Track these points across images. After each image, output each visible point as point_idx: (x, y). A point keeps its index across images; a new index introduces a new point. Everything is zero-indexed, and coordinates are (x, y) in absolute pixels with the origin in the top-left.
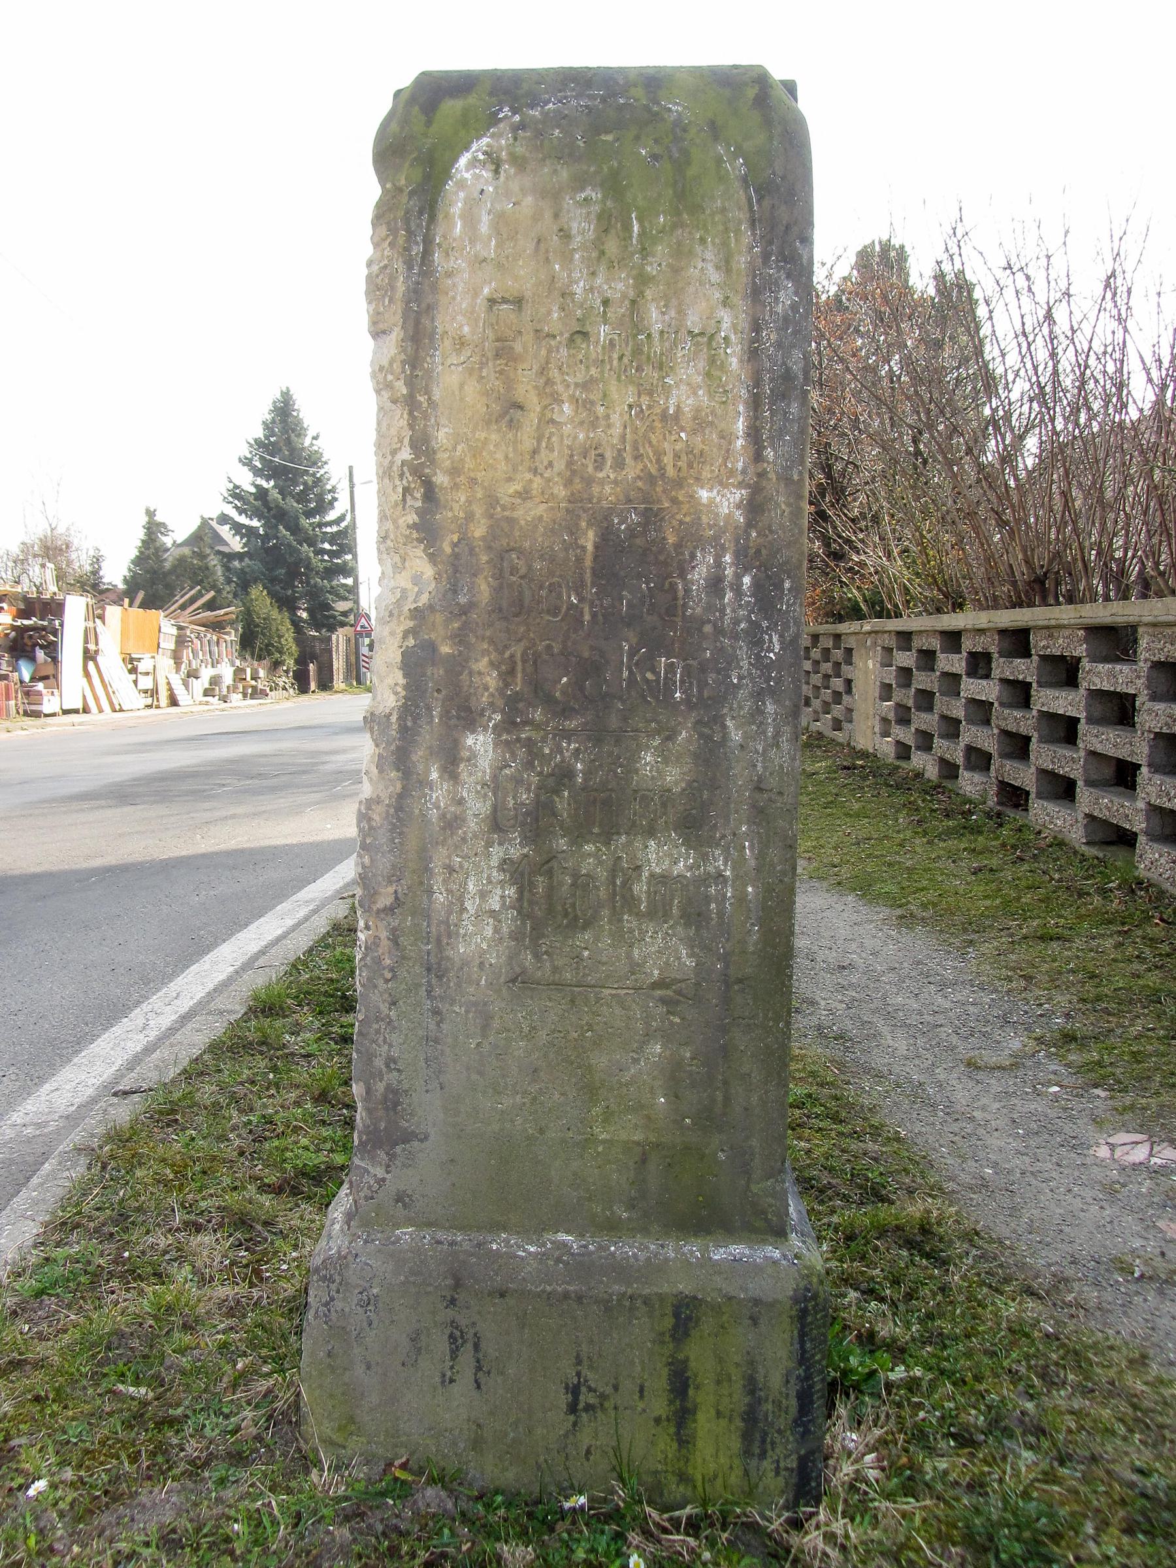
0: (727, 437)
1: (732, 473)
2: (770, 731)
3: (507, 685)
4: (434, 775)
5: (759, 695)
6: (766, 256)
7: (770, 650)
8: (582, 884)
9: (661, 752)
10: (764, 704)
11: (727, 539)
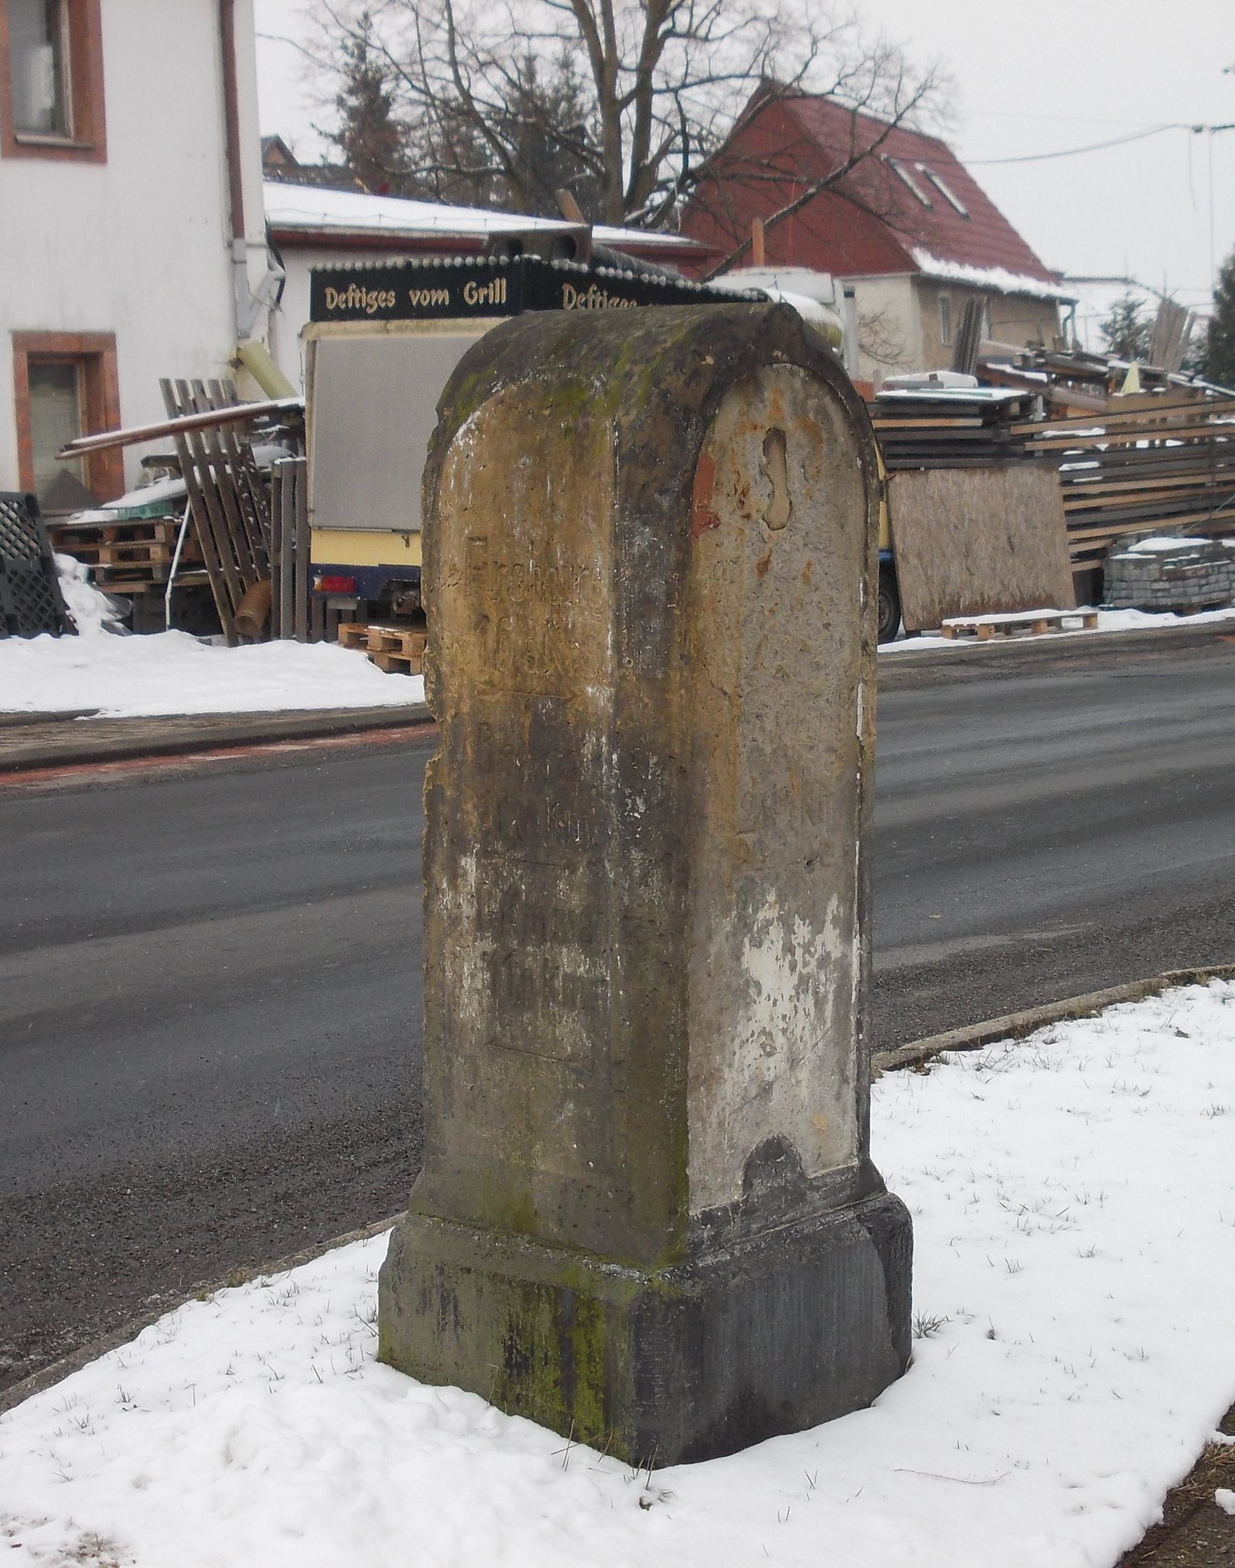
0: (601, 647)
1: (605, 674)
2: (637, 872)
3: (483, 823)
4: (445, 886)
5: (625, 846)
6: (622, 510)
7: (634, 810)
8: (526, 976)
9: (570, 883)
10: (629, 851)
11: (603, 725)
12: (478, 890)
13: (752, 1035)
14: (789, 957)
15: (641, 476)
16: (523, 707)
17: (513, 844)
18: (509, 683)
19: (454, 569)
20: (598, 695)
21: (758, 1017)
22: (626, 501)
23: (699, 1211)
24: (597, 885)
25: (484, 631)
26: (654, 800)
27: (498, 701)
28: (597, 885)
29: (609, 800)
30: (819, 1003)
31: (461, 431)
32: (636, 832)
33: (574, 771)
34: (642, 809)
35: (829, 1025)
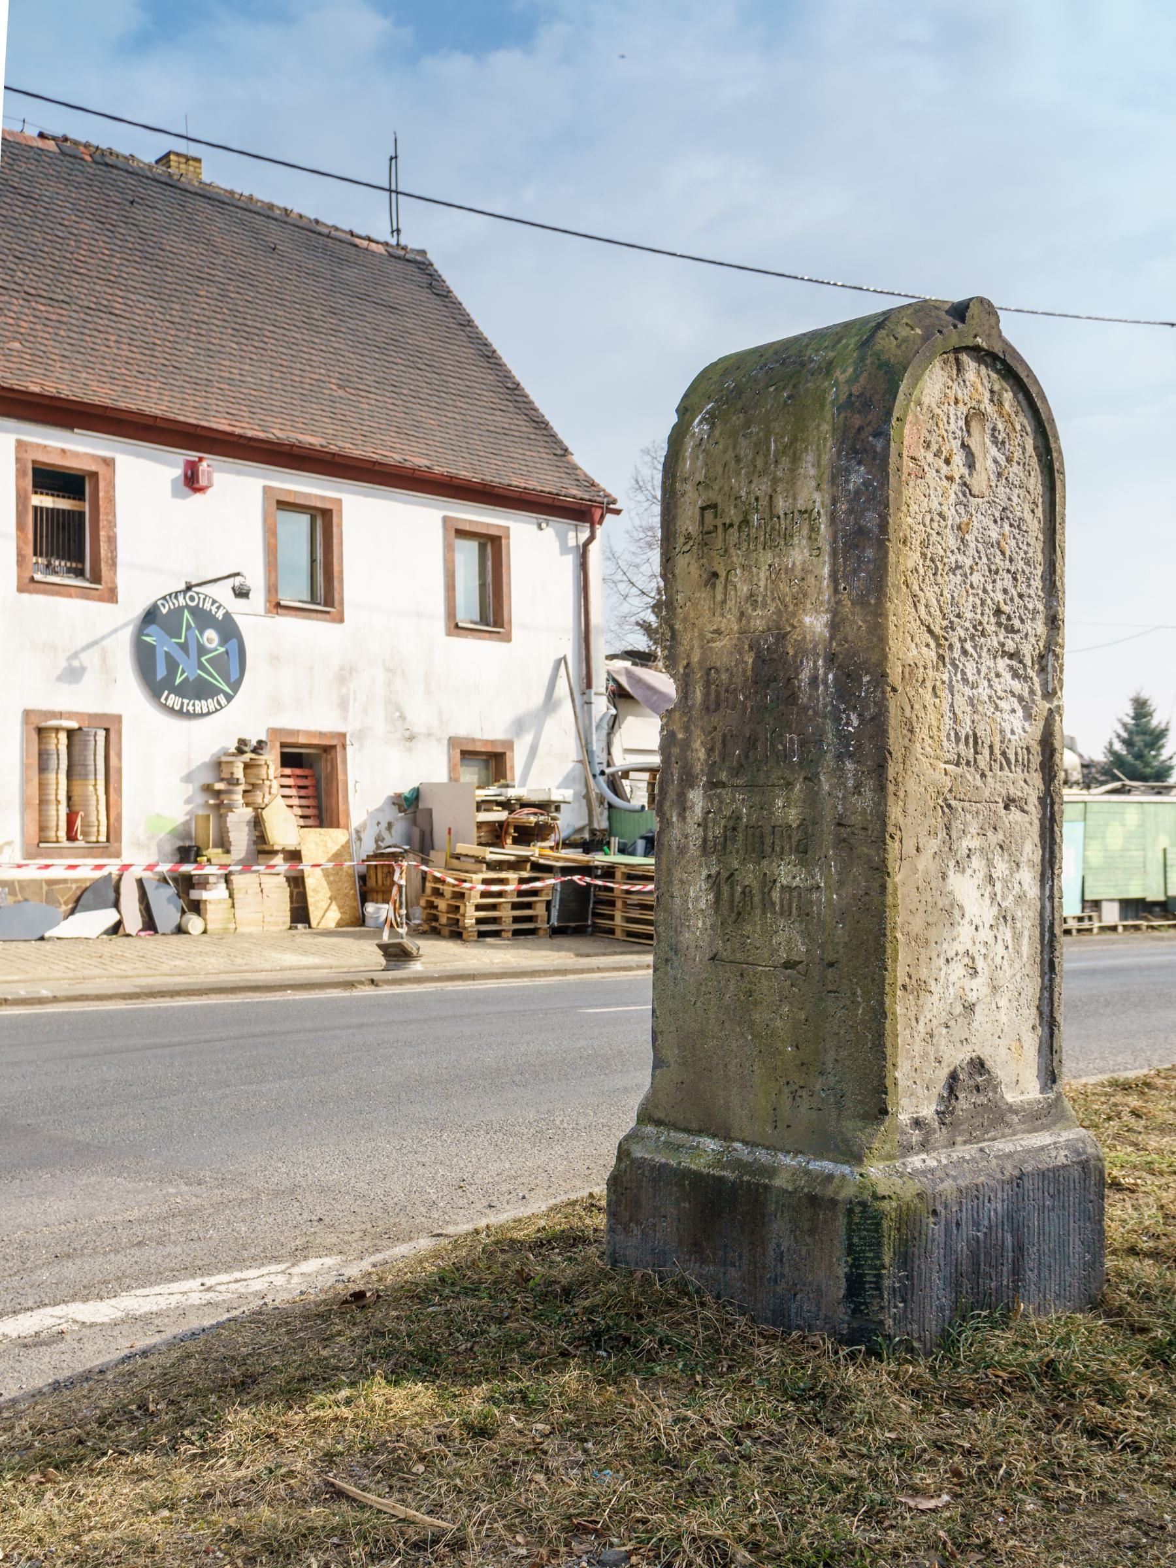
4: (674, 819)
5: (839, 757)
6: (839, 452)
8: (746, 892)
10: (843, 763)
12: (705, 819)
13: (957, 955)
14: (989, 888)
15: (857, 421)
16: (746, 647)
17: (736, 772)
18: (736, 627)
19: (689, 537)
20: (815, 623)
21: (962, 939)
22: (843, 443)
23: (907, 1116)
24: (812, 799)
25: (714, 586)
26: (867, 715)
27: (724, 646)
28: (812, 799)
29: (825, 717)
30: (1017, 937)
31: (697, 421)
32: (850, 745)
33: (792, 698)
34: (856, 723)
35: (1025, 959)
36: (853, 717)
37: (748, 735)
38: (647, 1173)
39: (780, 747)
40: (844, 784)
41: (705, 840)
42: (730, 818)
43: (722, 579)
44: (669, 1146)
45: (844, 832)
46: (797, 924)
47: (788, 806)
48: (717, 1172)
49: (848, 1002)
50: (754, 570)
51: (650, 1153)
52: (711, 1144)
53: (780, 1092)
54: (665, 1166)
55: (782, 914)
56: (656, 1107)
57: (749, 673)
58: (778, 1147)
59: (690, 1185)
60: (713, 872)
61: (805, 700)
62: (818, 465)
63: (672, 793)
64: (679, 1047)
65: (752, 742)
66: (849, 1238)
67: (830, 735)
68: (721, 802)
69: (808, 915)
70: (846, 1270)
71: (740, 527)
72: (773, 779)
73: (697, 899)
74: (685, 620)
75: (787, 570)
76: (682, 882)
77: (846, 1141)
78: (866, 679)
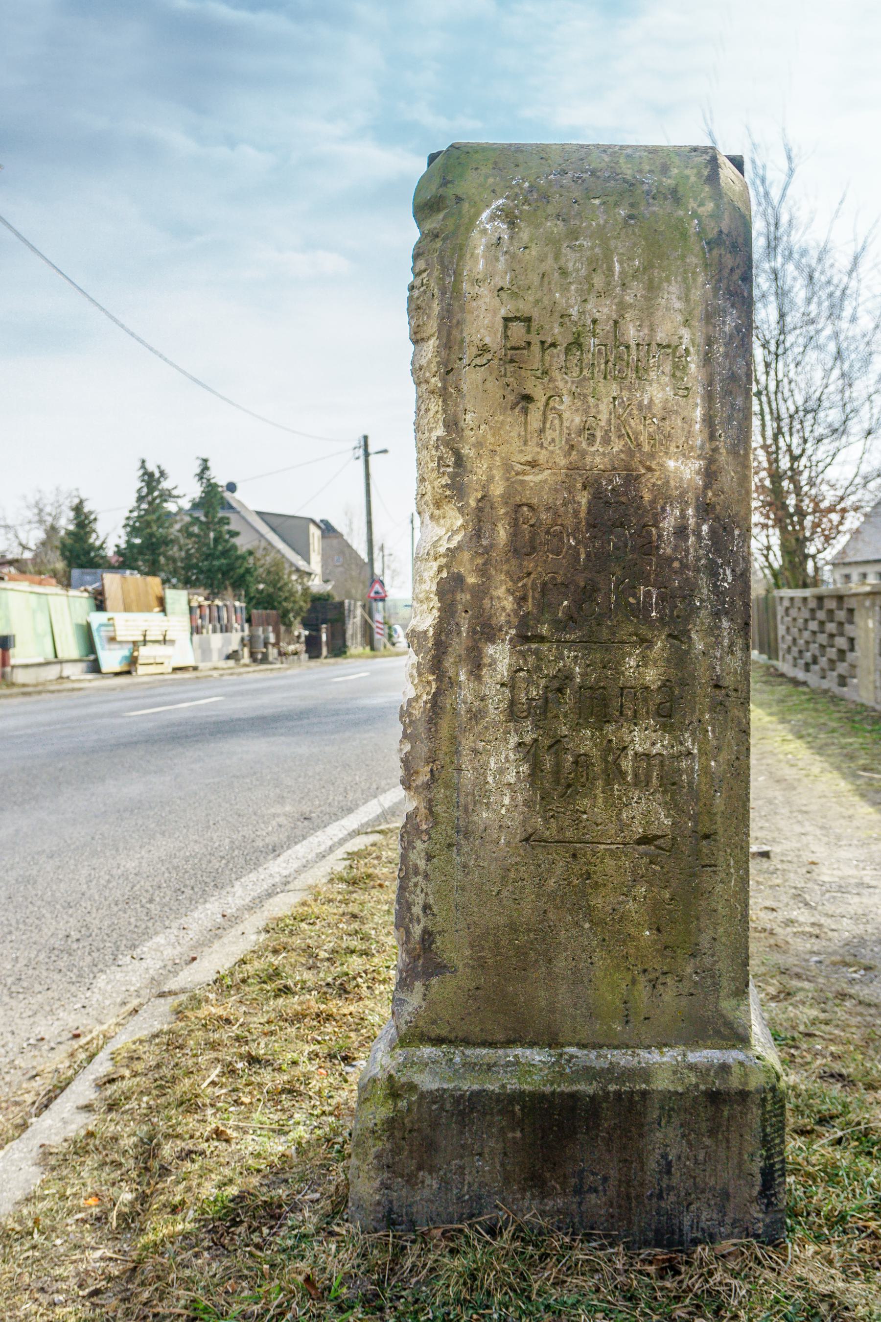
4: (462, 678)
5: (717, 615)
6: (716, 290)
10: (720, 621)
12: (513, 678)
16: (579, 486)
19: (484, 349)
22: (720, 280)
25: (525, 411)
27: (546, 481)
34: (730, 579)
36: (728, 572)
37: (582, 584)
38: (448, 1106)
39: (631, 600)
40: (721, 643)
41: (512, 703)
42: (555, 677)
43: (541, 404)
44: (470, 1066)
45: (720, 694)
46: (658, 795)
47: (645, 665)
48: (565, 1088)
49: (724, 875)
50: (591, 401)
51: (449, 1081)
52: (537, 1056)
53: (634, 982)
54: (477, 1095)
55: (635, 785)
56: (434, 1022)
57: (583, 515)
58: (631, 1044)
59: (522, 1110)
60: (528, 739)
61: (669, 551)
62: (686, 298)
63: (458, 645)
64: (472, 947)
65: (589, 593)
66: (764, 1130)
67: (705, 591)
68: (539, 659)
69: (674, 784)
70: (762, 1164)
71: (568, 350)
72: (622, 634)
73: (501, 771)
74: (479, 445)
75: (640, 407)
76: (475, 751)
77: (728, 1024)
78: (737, 532)
